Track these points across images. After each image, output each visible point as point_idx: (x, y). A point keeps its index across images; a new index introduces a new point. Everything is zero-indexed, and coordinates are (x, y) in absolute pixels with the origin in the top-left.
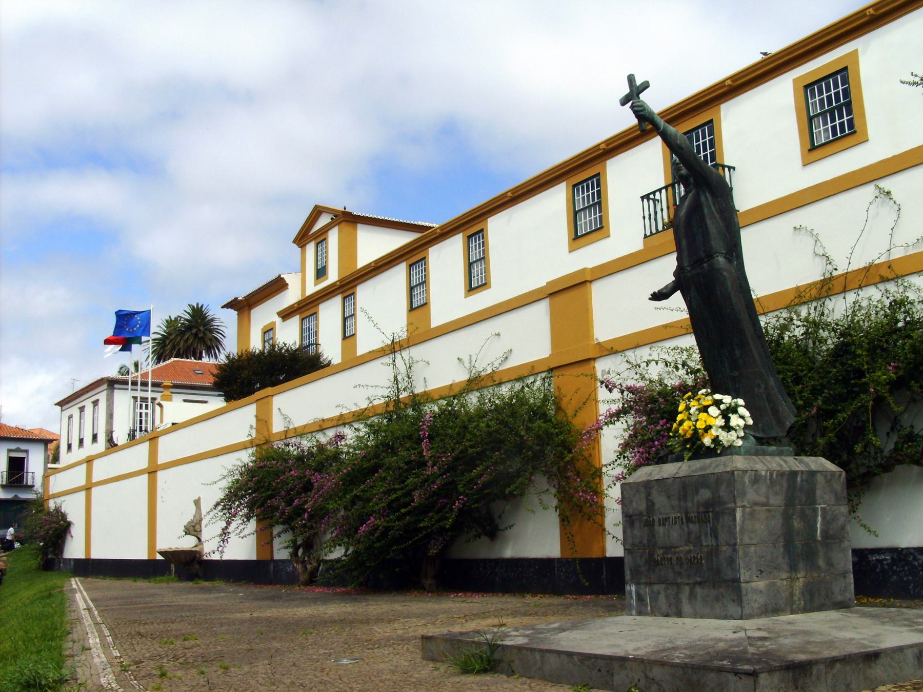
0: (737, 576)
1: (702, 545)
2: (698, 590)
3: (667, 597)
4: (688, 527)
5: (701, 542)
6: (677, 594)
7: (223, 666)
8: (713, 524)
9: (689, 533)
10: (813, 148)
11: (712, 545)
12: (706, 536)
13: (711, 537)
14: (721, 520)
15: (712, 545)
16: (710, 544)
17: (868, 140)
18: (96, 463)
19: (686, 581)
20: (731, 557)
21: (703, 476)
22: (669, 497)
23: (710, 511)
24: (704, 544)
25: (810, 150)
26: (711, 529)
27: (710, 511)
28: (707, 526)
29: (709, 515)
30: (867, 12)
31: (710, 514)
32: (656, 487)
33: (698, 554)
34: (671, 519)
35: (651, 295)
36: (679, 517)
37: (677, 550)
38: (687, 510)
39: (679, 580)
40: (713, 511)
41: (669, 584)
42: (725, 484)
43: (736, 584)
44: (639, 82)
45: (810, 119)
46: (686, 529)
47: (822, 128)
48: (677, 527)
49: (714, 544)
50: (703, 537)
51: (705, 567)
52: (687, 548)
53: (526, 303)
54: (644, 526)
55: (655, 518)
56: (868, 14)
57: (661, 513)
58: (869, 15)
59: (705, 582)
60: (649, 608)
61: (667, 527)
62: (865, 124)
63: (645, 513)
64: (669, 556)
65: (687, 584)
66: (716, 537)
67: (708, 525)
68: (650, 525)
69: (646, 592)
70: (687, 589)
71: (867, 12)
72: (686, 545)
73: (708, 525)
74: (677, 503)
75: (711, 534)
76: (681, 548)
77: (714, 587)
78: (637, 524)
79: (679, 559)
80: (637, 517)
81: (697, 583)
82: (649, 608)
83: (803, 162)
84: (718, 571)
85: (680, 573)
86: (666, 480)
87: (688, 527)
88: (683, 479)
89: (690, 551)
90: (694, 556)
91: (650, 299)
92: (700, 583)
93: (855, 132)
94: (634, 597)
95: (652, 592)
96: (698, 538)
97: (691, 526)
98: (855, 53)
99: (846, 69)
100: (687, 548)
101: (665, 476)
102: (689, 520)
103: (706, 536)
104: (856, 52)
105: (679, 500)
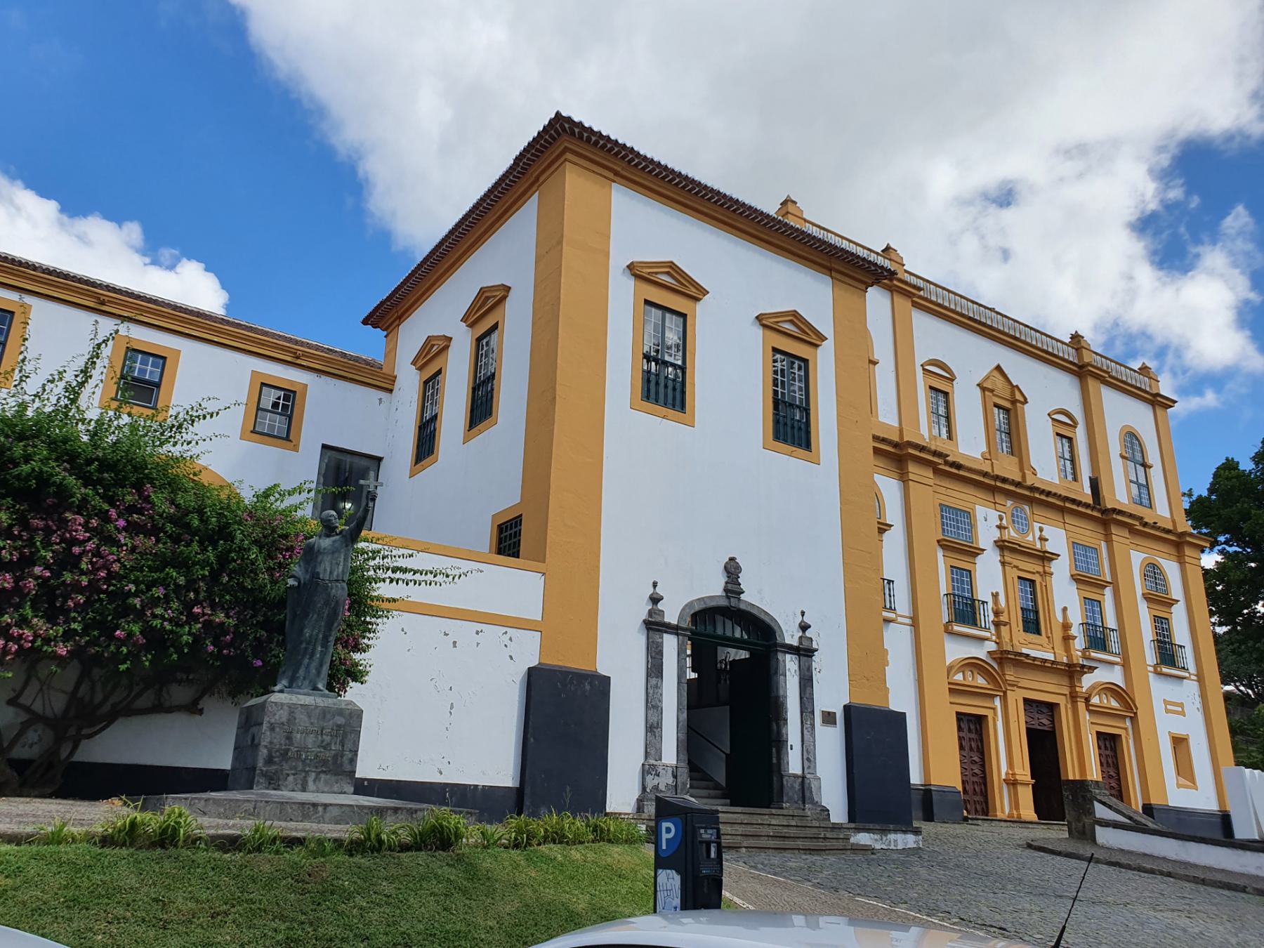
6: (305, 777)
9: (323, 741)
22: (309, 717)
46: (320, 738)
66: (343, 746)
89: (321, 752)
105: (318, 719)
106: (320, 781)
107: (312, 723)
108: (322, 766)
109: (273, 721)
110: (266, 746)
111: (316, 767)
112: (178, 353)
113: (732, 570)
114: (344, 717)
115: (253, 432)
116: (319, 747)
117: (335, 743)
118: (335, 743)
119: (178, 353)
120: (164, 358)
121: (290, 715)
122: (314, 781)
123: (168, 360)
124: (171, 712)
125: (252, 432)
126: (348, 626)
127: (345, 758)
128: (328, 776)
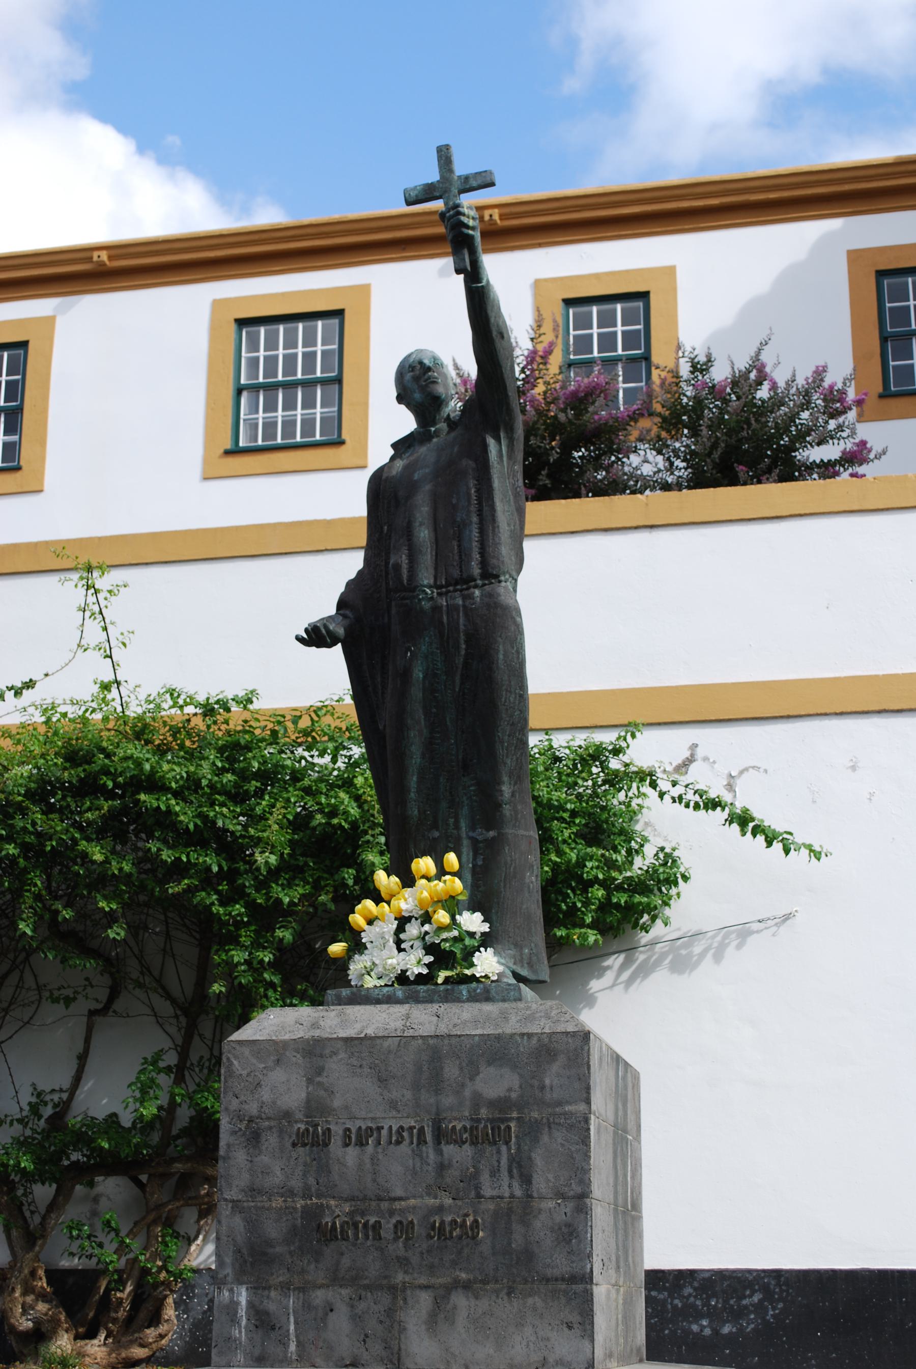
0: (584, 1267)
1: (479, 1196)
2: (460, 1300)
3: (356, 1319)
4: (440, 1152)
5: (478, 1188)
6: (390, 1312)
7: (565, 1321)
8: (519, 1149)
9: (442, 1167)
10: (234, 451)
11: (512, 1196)
12: (494, 1173)
13: (511, 1176)
14: (545, 1138)
15: (512, 1196)
16: (507, 1195)
17: (41, 491)
18: (110, 660)
19: (423, 1280)
20: (568, 1225)
21: (498, 1037)
22: (382, 1081)
23: (511, 1119)
24: (487, 1191)
25: (228, 453)
26: (511, 1160)
27: (511, 1119)
28: (499, 1152)
29: (509, 1128)
30: (95, 255)
31: (513, 1125)
32: (342, 1055)
33: (467, 1215)
34: (384, 1132)
35: (306, 630)
36: (411, 1128)
37: (397, 1205)
38: (438, 1114)
39: (400, 1277)
40: (518, 1119)
41: (367, 1287)
42: (562, 1059)
43: (579, 1287)
44: (462, 167)
45: (239, 391)
46: (432, 1156)
47: (280, 412)
48: (405, 1148)
49: (518, 1192)
50: (485, 1178)
51: (485, 1248)
52: (431, 1201)
53: (686, 521)
54: (294, 1145)
55: (333, 1127)
56: (95, 258)
57: (353, 1118)
58: (97, 262)
59: (485, 1282)
60: (293, 1347)
61: (370, 1149)
62: (42, 459)
63: (299, 1116)
64: (372, 1220)
65: (426, 1287)
66: (527, 1180)
67: (504, 1148)
68: (316, 1143)
69: (287, 1308)
70: (425, 1299)
71: (95, 255)
72: (429, 1194)
73: (504, 1148)
74: (408, 1095)
75: (510, 1172)
76: (412, 1202)
77: (509, 1294)
78: (271, 1140)
79: (366, 1225)
80: (272, 1123)
81: (457, 1285)
82: (293, 1347)
83: (204, 470)
84: (528, 1256)
85: (404, 1263)
86: (378, 1041)
87: (440, 1152)
88: (431, 1042)
89: (440, 1209)
90: (455, 1221)
91: (299, 639)
92: (467, 1286)
93: (18, 468)
94: (244, 1322)
95: (308, 1306)
96: (471, 1180)
97: (449, 1150)
98: (49, 322)
99: (24, 345)
100: (431, 1201)
101: (370, 1031)
102: (441, 1136)
103: (494, 1173)
104: (49, 322)
105: (416, 1087)
106: (451, 1320)
107: (393, 1105)
108: (454, 1263)
109: (253, 1109)
110: (236, 1205)
111: (432, 1269)
112: (670, 272)
113: (709, 348)
114: (514, 1067)
115: (886, 395)
116: (430, 1191)
117: (495, 1172)
118: (495, 1172)
119: (670, 272)
120: (644, 296)
121: (310, 1081)
122: (432, 1322)
123: (653, 297)
124: (636, 1206)
125: (881, 396)
126: (118, 743)
127: (537, 1224)
128: (484, 1304)
